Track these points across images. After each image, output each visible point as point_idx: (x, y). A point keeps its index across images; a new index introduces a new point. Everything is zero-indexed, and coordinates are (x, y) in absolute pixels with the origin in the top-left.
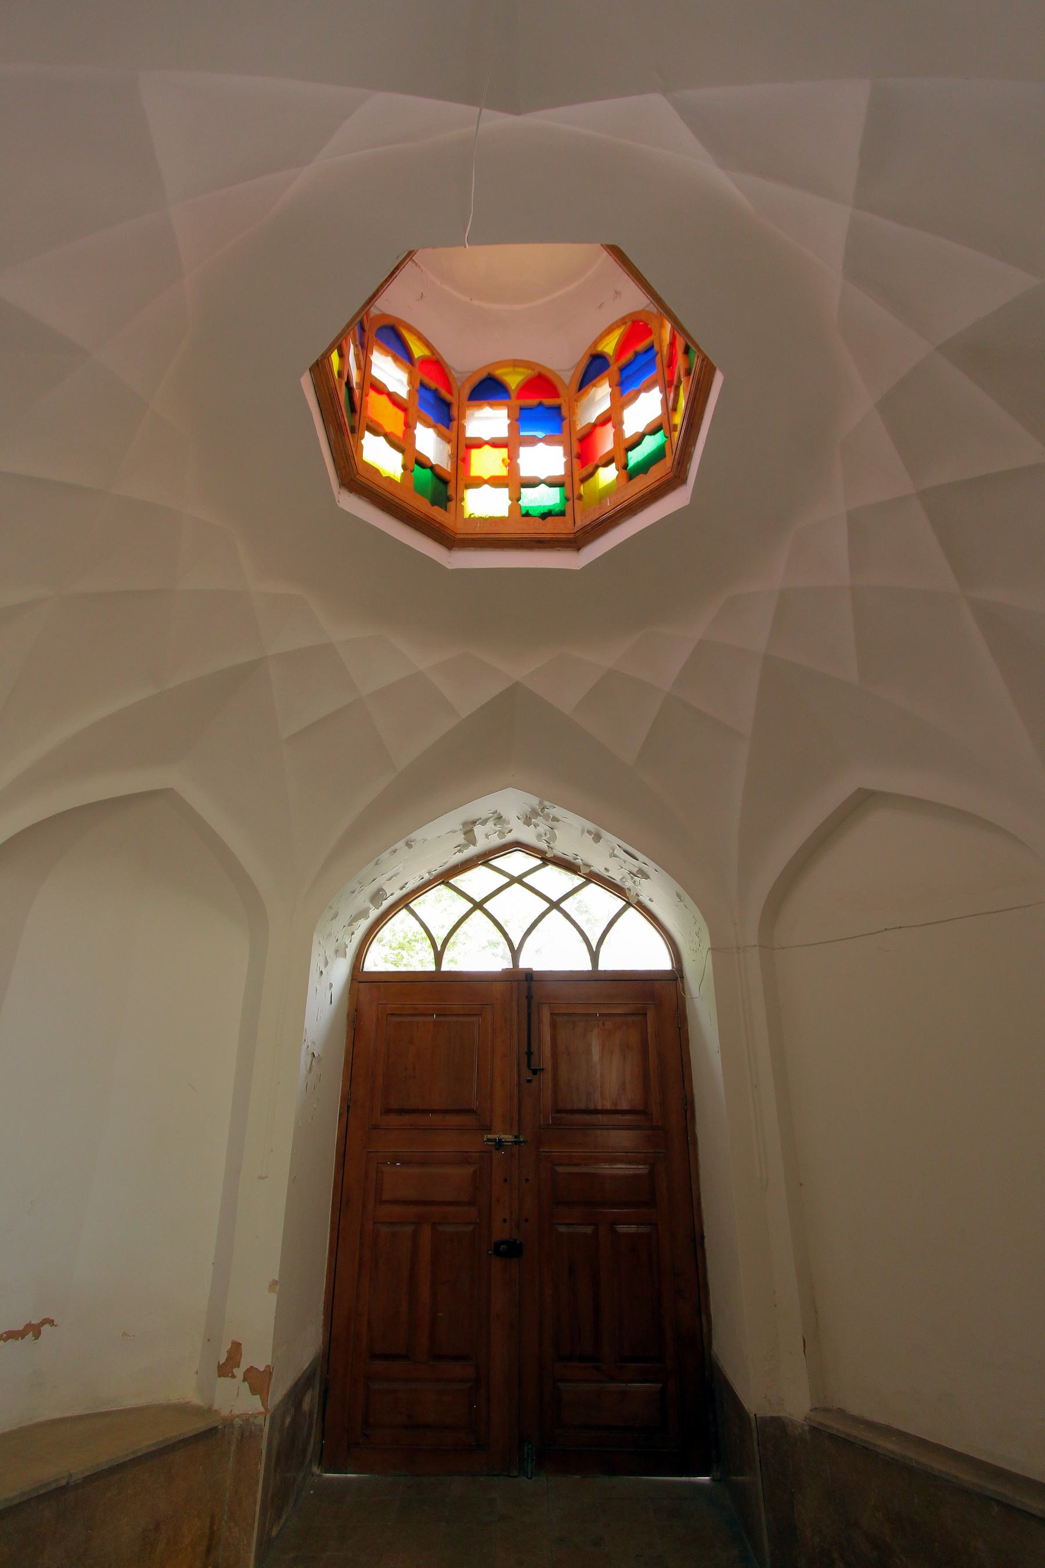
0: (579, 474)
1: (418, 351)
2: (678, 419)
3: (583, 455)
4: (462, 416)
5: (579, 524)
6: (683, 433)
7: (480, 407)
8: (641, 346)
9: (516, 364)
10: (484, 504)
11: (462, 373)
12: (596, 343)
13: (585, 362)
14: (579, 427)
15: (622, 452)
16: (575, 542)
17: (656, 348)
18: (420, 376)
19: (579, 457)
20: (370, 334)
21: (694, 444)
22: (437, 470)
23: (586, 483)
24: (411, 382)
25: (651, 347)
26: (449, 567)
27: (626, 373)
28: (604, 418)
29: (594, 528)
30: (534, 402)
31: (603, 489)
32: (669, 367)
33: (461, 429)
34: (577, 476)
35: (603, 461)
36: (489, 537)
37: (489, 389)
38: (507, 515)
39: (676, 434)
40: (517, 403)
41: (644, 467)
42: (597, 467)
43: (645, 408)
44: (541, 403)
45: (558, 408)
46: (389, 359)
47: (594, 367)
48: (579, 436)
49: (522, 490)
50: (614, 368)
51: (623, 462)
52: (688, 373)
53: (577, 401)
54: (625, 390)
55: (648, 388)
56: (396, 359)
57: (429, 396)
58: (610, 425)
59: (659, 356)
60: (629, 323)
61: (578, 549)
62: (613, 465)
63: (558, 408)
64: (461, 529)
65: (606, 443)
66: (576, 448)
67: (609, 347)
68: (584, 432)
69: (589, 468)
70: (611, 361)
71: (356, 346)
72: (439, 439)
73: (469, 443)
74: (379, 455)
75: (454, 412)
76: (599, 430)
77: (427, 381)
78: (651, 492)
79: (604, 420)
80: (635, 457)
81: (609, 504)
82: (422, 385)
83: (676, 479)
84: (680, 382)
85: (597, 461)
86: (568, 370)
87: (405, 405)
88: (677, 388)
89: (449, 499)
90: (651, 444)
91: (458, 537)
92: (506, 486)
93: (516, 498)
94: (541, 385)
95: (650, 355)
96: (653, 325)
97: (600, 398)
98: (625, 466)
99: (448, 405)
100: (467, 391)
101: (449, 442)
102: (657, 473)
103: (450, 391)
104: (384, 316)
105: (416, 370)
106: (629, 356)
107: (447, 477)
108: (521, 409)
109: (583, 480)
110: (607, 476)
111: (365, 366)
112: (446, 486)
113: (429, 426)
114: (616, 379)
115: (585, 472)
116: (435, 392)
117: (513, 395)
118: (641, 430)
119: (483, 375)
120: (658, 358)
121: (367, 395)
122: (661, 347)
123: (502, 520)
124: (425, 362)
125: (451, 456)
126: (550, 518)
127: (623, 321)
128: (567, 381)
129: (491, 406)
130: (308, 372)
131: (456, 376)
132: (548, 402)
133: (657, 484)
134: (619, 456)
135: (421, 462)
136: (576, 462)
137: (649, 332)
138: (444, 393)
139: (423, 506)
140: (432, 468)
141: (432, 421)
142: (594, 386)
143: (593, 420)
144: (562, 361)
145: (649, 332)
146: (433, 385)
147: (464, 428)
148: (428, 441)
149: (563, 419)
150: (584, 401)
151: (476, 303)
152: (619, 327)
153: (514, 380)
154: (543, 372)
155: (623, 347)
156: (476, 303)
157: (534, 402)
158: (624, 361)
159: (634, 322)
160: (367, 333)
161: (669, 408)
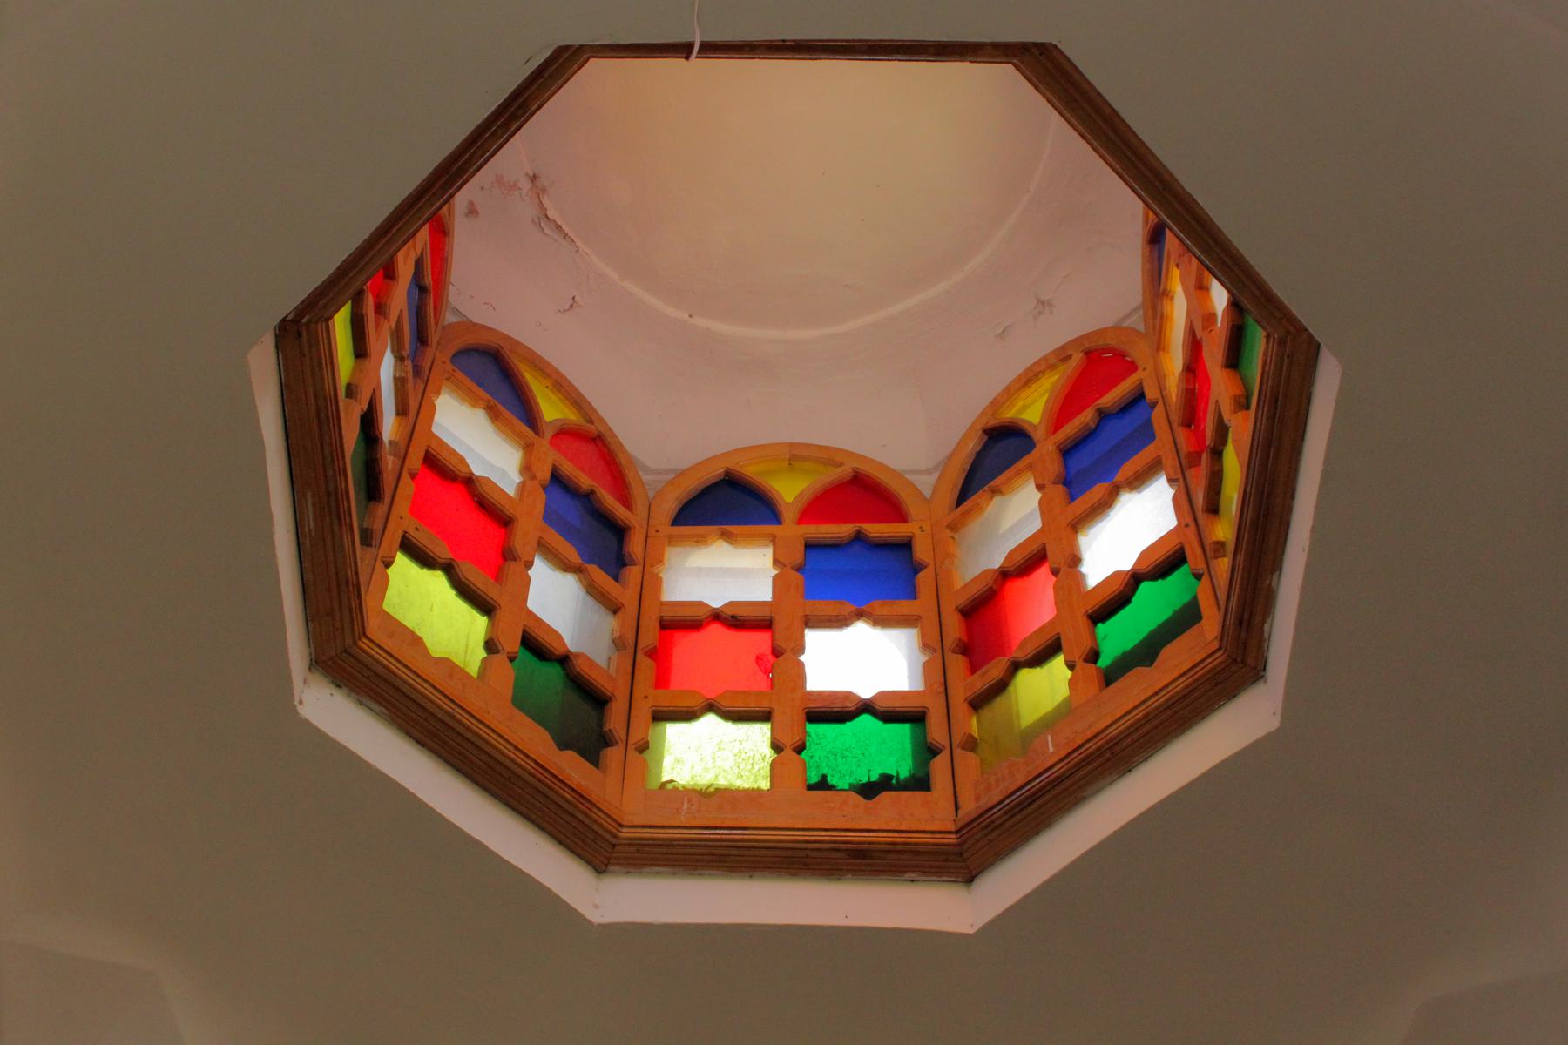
0: (964, 684)
1: (552, 410)
2: (1224, 530)
3: (977, 639)
4: (652, 560)
5: (969, 807)
6: (1236, 558)
7: (701, 541)
8: (1112, 398)
9: (796, 456)
10: (709, 755)
11: (659, 472)
12: (996, 404)
13: (973, 446)
14: (959, 583)
15: (1083, 623)
16: (961, 857)
17: (1151, 393)
18: (549, 458)
19: (965, 649)
20: (439, 355)
21: (1277, 566)
22: (581, 667)
23: (986, 712)
24: (527, 469)
25: (1138, 397)
26: (596, 917)
27: (1082, 459)
28: (1026, 553)
29: (1012, 812)
30: (844, 530)
31: (1029, 727)
32: (1187, 423)
33: (649, 585)
34: (959, 695)
35: (1030, 650)
36: (715, 841)
37: (726, 502)
38: (765, 784)
39: (1223, 565)
40: (793, 531)
41: (1147, 652)
42: (1016, 667)
43: (1131, 527)
44: (859, 542)
45: (905, 546)
46: (479, 417)
47: (997, 449)
48: (962, 600)
49: (812, 728)
50: (1046, 449)
51: (1086, 644)
52: (1242, 404)
53: (954, 527)
54: (1086, 481)
55: (1137, 481)
56: (494, 415)
57: (572, 511)
58: (1044, 571)
59: (1159, 409)
60: (1077, 358)
61: (969, 879)
62: (1058, 664)
63: (905, 546)
64: (633, 813)
65: (1037, 607)
66: (955, 628)
67: (1032, 410)
68: (975, 591)
69: (995, 670)
70: (1038, 436)
71: (400, 358)
72: (590, 601)
73: (668, 614)
74: (427, 608)
75: (635, 546)
76: (1016, 587)
77: (568, 469)
78: (1169, 705)
79: (1030, 561)
80: (1118, 635)
81: (1052, 749)
82: (557, 478)
83: (1238, 665)
84: (1222, 431)
85: (1019, 655)
86: (928, 472)
87: (509, 510)
88: (1217, 454)
89: (606, 741)
90: (1153, 605)
91: (625, 833)
92: (764, 717)
93: (788, 748)
94: (860, 494)
95: (1133, 419)
96: (1139, 352)
97: (1017, 513)
98: (1094, 656)
99: (620, 532)
100: (670, 505)
101: (615, 610)
102: (1179, 658)
103: (626, 501)
104: (471, 326)
105: (543, 445)
106: (1087, 417)
107: (602, 683)
108: (810, 546)
109: (978, 703)
110: (1044, 689)
111: (414, 409)
112: (591, 712)
113: (566, 567)
114: (1054, 466)
115: (981, 681)
116: (586, 499)
117: (789, 515)
118: (1127, 564)
119: (715, 473)
120: (1158, 415)
121: (388, 564)
122: (1161, 388)
123: (752, 796)
124: (565, 433)
125: (618, 643)
126: (886, 797)
127: (1062, 355)
128: (926, 484)
129: (729, 538)
130: (269, 341)
131: (646, 478)
132: (876, 530)
133: (1182, 683)
134: (1075, 634)
135: (537, 644)
136: (958, 663)
137: (1132, 367)
138: (609, 501)
139: (532, 740)
140: (564, 660)
141: (574, 556)
142: (995, 491)
143: (997, 561)
144: (911, 444)
145: (1132, 367)
146: (585, 481)
147: (657, 583)
148: (554, 596)
149: (917, 568)
150: (974, 527)
151: (701, 322)
152: (1052, 367)
153: (790, 490)
154: (866, 468)
155: (1063, 411)
156: (701, 322)
157: (844, 530)
158: (1070, 429)
159: (1088, 353)
160: (429, 353)
161: (1197, 505)
